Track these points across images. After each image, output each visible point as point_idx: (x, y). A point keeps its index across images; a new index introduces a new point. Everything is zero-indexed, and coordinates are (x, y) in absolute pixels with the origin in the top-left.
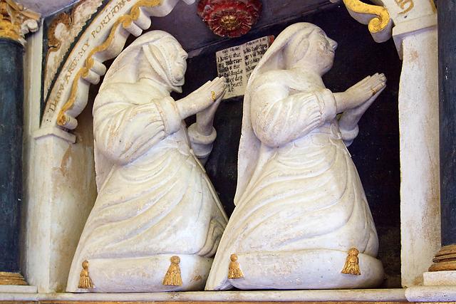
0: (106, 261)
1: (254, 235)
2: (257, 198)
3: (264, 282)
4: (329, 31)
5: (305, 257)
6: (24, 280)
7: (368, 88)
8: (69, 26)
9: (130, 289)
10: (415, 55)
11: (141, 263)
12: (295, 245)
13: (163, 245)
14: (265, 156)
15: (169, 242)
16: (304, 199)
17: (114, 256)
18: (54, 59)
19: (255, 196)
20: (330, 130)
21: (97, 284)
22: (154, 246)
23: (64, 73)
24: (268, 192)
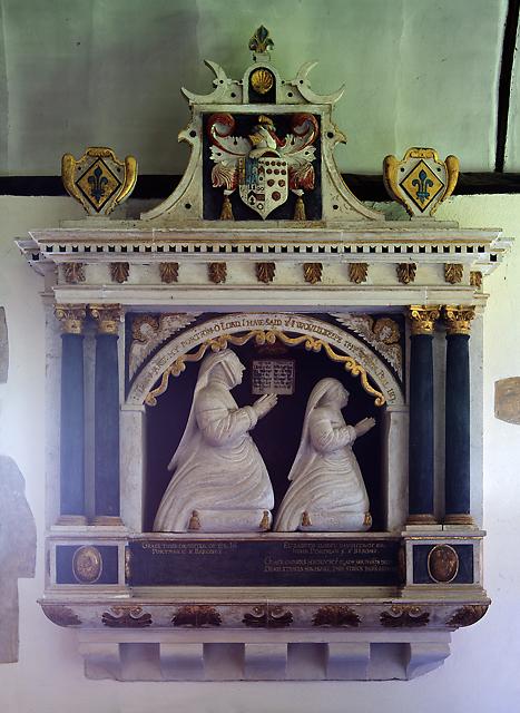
0: (214, 512)
1: (318, 502)
2: (317, 482)
3: (326, 528)
4: (346, 386)
5: (348, 516)
6: (120, 522)
7: (367, 424)
8: (157, 328)
9: (230, 530)
10: (396, 422)
11: (246, 515)
12: (341, 509)
13: (259, 504)
14: (315, 455)
15: (263, 502)
16: (344, 485)
17: (223, 509)
18: (138, 350)
19: (313, 480)
20: (470, 519)
21: (204, 526)
22: (254, 505)
23: (152, 365)
24: (322, 479)
